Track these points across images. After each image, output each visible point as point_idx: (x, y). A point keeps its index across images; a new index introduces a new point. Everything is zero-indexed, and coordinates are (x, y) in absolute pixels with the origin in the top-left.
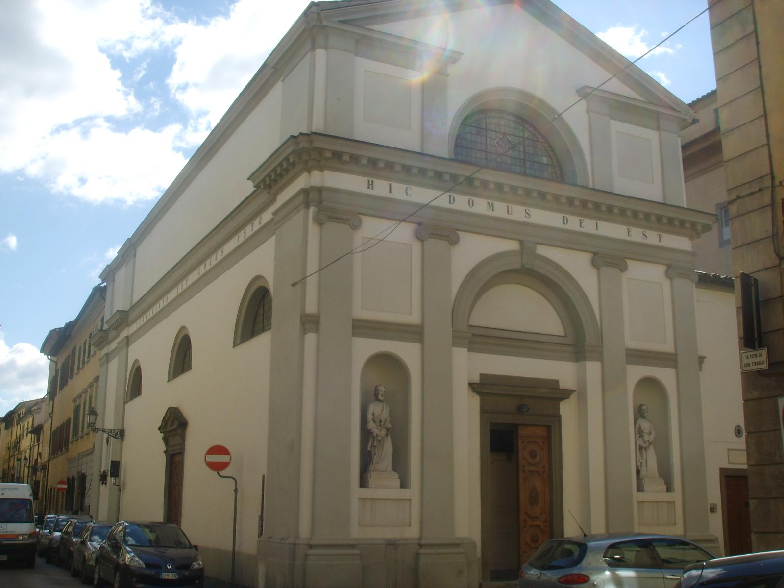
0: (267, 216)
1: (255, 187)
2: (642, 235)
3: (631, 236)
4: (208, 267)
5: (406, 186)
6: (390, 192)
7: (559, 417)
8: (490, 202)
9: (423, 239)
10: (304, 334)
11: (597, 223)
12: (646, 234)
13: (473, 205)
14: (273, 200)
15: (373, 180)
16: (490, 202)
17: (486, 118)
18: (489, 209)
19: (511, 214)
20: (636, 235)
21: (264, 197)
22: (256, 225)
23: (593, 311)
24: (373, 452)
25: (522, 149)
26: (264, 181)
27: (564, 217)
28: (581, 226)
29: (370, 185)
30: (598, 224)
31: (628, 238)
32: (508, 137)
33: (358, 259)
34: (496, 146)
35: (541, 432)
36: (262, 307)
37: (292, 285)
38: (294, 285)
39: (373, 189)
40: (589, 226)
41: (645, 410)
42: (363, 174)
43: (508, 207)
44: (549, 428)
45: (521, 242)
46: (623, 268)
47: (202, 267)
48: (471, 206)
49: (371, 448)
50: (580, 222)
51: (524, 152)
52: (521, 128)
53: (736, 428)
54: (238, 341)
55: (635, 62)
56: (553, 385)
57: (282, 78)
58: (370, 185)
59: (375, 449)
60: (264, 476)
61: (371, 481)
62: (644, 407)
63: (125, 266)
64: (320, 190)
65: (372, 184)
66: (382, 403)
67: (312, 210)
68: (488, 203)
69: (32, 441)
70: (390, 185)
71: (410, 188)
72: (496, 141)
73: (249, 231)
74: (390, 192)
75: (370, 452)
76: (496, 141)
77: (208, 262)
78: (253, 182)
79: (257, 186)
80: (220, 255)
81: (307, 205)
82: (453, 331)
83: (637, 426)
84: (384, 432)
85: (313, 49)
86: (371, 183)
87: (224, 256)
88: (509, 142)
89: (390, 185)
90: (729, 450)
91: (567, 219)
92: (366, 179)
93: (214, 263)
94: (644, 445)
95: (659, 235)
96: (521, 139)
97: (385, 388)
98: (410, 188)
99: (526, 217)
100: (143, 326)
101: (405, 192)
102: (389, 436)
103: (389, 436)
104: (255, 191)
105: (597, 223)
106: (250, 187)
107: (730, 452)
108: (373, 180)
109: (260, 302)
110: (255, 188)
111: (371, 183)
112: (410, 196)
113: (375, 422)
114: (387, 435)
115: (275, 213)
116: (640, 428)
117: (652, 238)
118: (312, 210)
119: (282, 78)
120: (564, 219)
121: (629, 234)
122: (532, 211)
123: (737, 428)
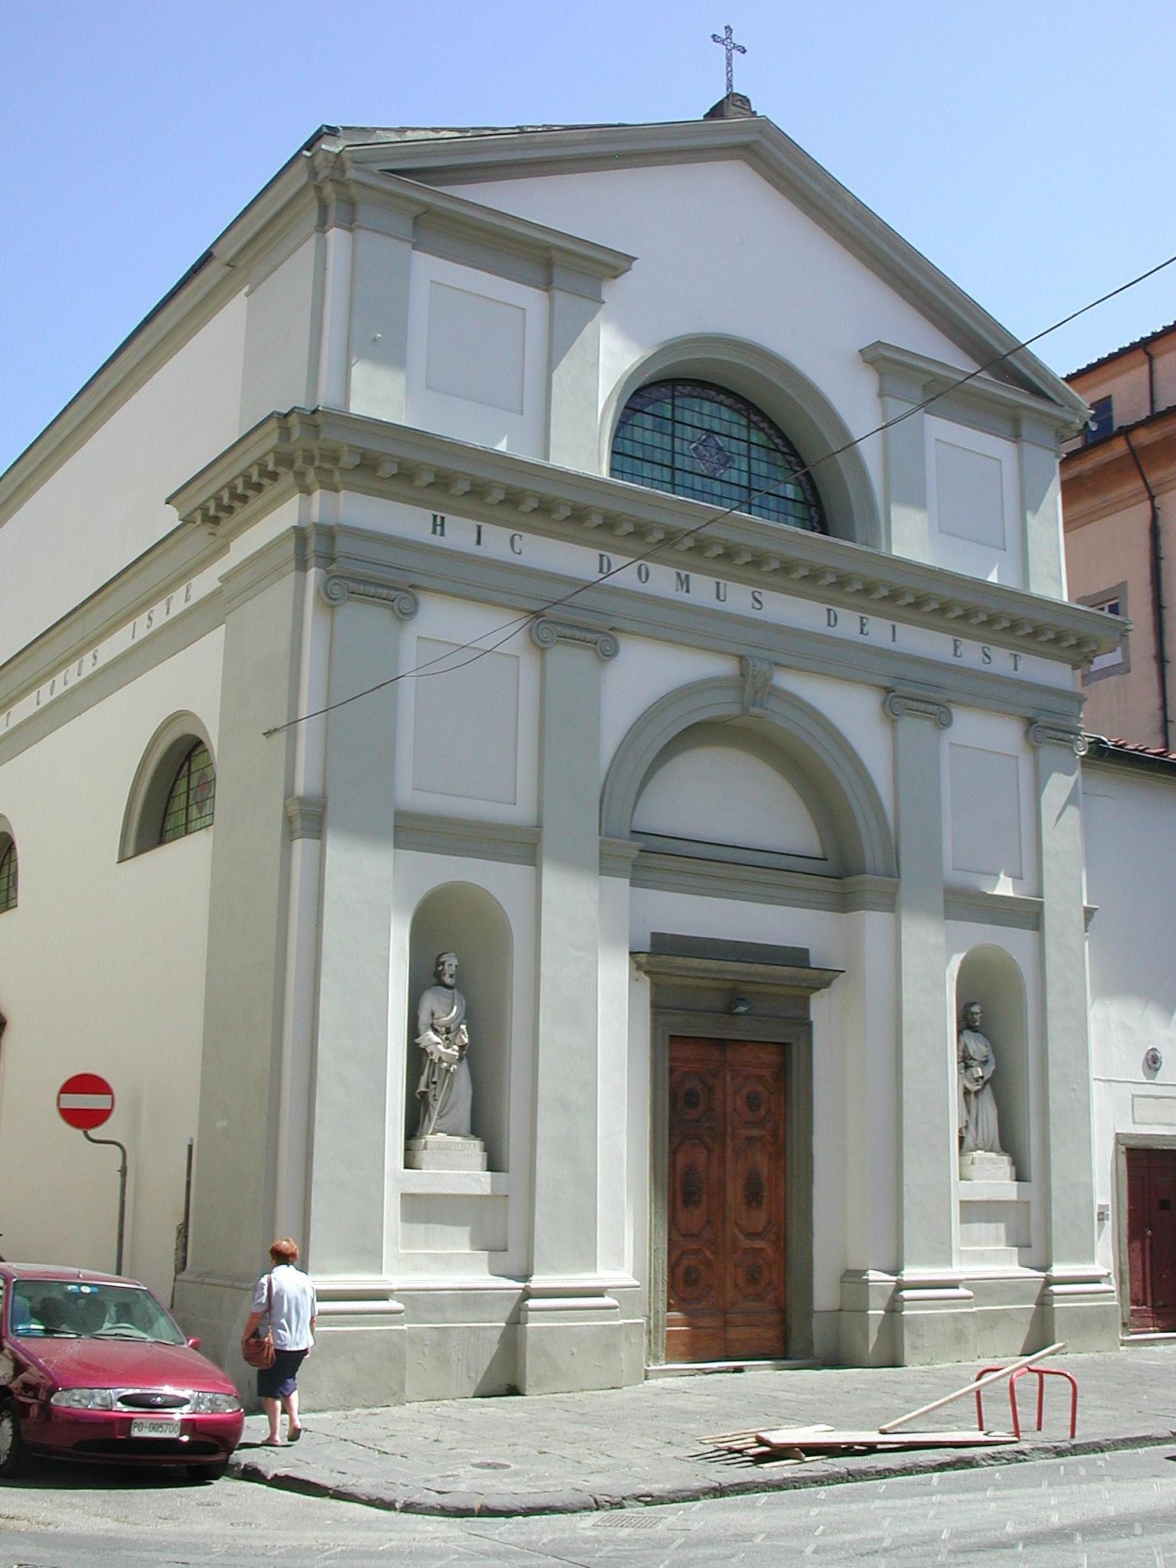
0: (205, 583)
1: (180, 520)
2: (982, 655)
3: (867, 635)
4: (60, 689)
5: (513, 532)
6: (479, 542)
7: (807, 1026)
8: (683, 573)
9: (545, 646)
10: (292, 840)
11: (894, 627)
12: (989, 654)
13: (647, 578)
14: (222, 550)
15: (443, 515)
16: (683, 573)
17: (673, 397)
18: (680, 587)
19: (724, 601)
20: (971, 654)
21: (201, 537)
22: (179, 602)
23: (881, 806)
24: (431, 1095)
25: (744, 467)
26: (203, 508)
27: (601, 556)
28: (862, 632)
29: (439, 525)
30: (483, 529)
31: (892, 646)
32: (717, 438)
33: (407, 688)
34: (693, 457)
35: (769, 1057)
36: (186, 779)
37: (265, 734)
38: (268, 734)
39: (442, 534)
40: (879, 631)
41: (977, 1013)
42: (822, 600)
43: (718, 583)
44: (783, 1048)
45: (742, 659)
46: (944, 722)
47: (45, 688)
48: (643, 579)
49: (428, 1087)
50: (955, 644)
51: (750, 473)
52: (744, 422)
53: (1147, 1054)
54: (130, 851)
55: (1152, 402)
56: (798, 957)
57: (246, 289)
58: (439, 525)
59: (435, 1089)
60: (190, 1147)
61: (423, 1156)
62: (976, 1009)
63: (247, 295)
64: (329, 533)
65: (442, 525)
66: (451, 991)
67: (313, 574)
68: (678, 574)
69: (684, 973)
70: (479, 527)
71: (521, 536)
72: (694, 445)
73: (160, 615)
74: (479, 542)
75: (424, 1094)
76: (694, 445)
77: (59, 678)
78: (178, 510)
79: (186, 521)
80: (88, 665)
81: (302, 565)
82: (601, 843)
83: (961, 1048)
84: (454, 1051)
85: (322, 226)
86: (439, 522)
87: (97, 667)
88: (720, 449)
89: (479, 527)
90: (1134, 1096)
91: (609, 562)
92: (429, 514)
93: (74, 680)
94: (974, 1087)
95: (1016, 656)
96: (678, 417)
97: (458, 961)
98: (521, 536)
99: (984, 662)
100: (74, 690)
101: (636, 574)
102: (465, 1061)
103: (465, 1061)
104: (178, 528)
105: (894, 627)
106: (171, 518)
107: (1136, 1099)
108: (688, 573)
109: (182, 766)
110: (180, 522)
111: (439, 522)
112: (520, 553)
113: (436, 1031)
114: (461, 1059)
115: (225, 579)
116: (966, 1046)
117: (1001, 661)
118: (313, 574)
119: (246, 289)
120: (829, 614)
121: (955, 651)
122: (766, 596)
123: (1152, 1053)
